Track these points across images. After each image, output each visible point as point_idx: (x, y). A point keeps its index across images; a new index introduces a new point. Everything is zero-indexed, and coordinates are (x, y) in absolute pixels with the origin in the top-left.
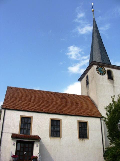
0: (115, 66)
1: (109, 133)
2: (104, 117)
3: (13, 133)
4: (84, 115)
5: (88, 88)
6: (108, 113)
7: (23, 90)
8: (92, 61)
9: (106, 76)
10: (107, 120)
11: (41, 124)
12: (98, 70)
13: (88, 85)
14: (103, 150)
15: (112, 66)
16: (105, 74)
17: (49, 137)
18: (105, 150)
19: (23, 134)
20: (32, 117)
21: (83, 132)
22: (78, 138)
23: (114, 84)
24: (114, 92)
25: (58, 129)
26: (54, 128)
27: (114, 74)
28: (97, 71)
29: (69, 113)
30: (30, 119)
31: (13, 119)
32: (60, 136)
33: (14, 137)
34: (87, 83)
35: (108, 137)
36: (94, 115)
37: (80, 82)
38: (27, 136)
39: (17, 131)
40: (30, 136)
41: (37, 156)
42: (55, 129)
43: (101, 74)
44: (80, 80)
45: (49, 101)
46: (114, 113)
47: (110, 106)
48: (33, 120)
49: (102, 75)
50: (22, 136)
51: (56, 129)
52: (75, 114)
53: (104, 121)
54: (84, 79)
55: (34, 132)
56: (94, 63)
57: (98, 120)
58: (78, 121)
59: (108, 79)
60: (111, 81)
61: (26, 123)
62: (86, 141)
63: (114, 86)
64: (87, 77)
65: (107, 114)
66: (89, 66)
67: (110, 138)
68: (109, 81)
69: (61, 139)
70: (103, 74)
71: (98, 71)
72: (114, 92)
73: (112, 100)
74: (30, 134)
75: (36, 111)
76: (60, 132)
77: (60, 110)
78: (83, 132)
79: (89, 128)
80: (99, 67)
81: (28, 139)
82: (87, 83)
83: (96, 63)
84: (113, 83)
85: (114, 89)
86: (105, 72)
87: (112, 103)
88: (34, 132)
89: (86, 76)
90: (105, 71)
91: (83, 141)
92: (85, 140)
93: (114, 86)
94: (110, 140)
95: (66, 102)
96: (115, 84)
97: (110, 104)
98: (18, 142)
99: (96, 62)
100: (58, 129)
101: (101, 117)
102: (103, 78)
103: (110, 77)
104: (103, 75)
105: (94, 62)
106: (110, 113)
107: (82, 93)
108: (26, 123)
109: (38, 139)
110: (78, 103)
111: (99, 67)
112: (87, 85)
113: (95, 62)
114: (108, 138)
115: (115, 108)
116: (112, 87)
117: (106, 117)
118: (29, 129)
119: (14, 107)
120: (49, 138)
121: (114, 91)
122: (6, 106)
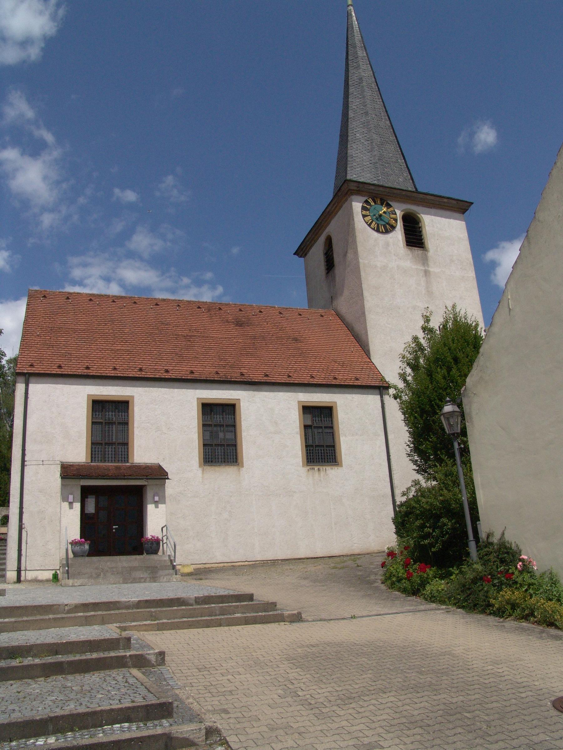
0: (432, 198)
2: (395, 388)
3: (64, 461)
5: (334, 279)
6: (409, 370)
7: (91, 300)
8: (346, 181)
9: (398, 235)
12: (367, 213)
16: (393, 228)
17: (200, 466)
18: (400, 499)
21: (320, 443)
22: (303, 466)
24: (430, 293)
25: (229, 436)
26: (213, 435)
28: (364, 216)
29: (267, 376)
30: (230, 408)
31: (55, 422)
32: (236, 462)
33: (69, 472)
34: (330, 264)
35: (409, 455)
36: (357, 379)
37: (302, 259)
38: (117, 468)
39: (78, 453)
40: (130, 467)
41: (160, 537)
42: (220, 440)
43: (378, 231)
44: (302, 251)
45: (191, 336)
46: (430, 374)
47: (413, 345)
49: (382, 233)
50: (98, 467)
51: (221, 435)
52: (288, 380)
54: (317, 251)
55: (144, 450)
56: (353, 186)
57: (372, 400)
58: (299, 402)
59: (407, 245)
60: (418, 252)
61: (110, 419)
62: (332, 472)
63: (427, 273)
64: (329, 241)
65: (403, 377)
66: (334, 198)
67: (416, 458)
69: (244, 469)
70: (388, 228)
72: (430, 293)
73: (421, 323)
74: (130, 461)
75: (143, 374)
76: (235, 446)
78: (320, 443)
80: (370, 200)
81: (124, 478)
82: (330, 264)
83: (360, 189)
84: (425, 261)
85: (428, 283)
86: (396, 220)
87: (421, 335)
88: (143, 452)
89: (322, 240)
91: (322, 473)
92: (328, 468)
93: (427, 273)
94: (415, 467)
95: (255, 338)
96: (431, 263)
97: (415, 339)
98: (86, 492)
100: (227, 437)
101: (382, 388)
102: (387, 244)
103: (415, 238)
104: (387, 232)
105: (352, 184)
106: (415, 367)
107: (360, 202)
108: (110, 419)
109: (157, 474)
110: (296, 340)
111: (373, 204)
113: (355, 184)
114: (410, 460)
115: (436, 351)
116: (422, 274)
117: (401, 385)
118: (123, 446)
119: (60, 367)
120: (200, 472)
121: (428, 291)
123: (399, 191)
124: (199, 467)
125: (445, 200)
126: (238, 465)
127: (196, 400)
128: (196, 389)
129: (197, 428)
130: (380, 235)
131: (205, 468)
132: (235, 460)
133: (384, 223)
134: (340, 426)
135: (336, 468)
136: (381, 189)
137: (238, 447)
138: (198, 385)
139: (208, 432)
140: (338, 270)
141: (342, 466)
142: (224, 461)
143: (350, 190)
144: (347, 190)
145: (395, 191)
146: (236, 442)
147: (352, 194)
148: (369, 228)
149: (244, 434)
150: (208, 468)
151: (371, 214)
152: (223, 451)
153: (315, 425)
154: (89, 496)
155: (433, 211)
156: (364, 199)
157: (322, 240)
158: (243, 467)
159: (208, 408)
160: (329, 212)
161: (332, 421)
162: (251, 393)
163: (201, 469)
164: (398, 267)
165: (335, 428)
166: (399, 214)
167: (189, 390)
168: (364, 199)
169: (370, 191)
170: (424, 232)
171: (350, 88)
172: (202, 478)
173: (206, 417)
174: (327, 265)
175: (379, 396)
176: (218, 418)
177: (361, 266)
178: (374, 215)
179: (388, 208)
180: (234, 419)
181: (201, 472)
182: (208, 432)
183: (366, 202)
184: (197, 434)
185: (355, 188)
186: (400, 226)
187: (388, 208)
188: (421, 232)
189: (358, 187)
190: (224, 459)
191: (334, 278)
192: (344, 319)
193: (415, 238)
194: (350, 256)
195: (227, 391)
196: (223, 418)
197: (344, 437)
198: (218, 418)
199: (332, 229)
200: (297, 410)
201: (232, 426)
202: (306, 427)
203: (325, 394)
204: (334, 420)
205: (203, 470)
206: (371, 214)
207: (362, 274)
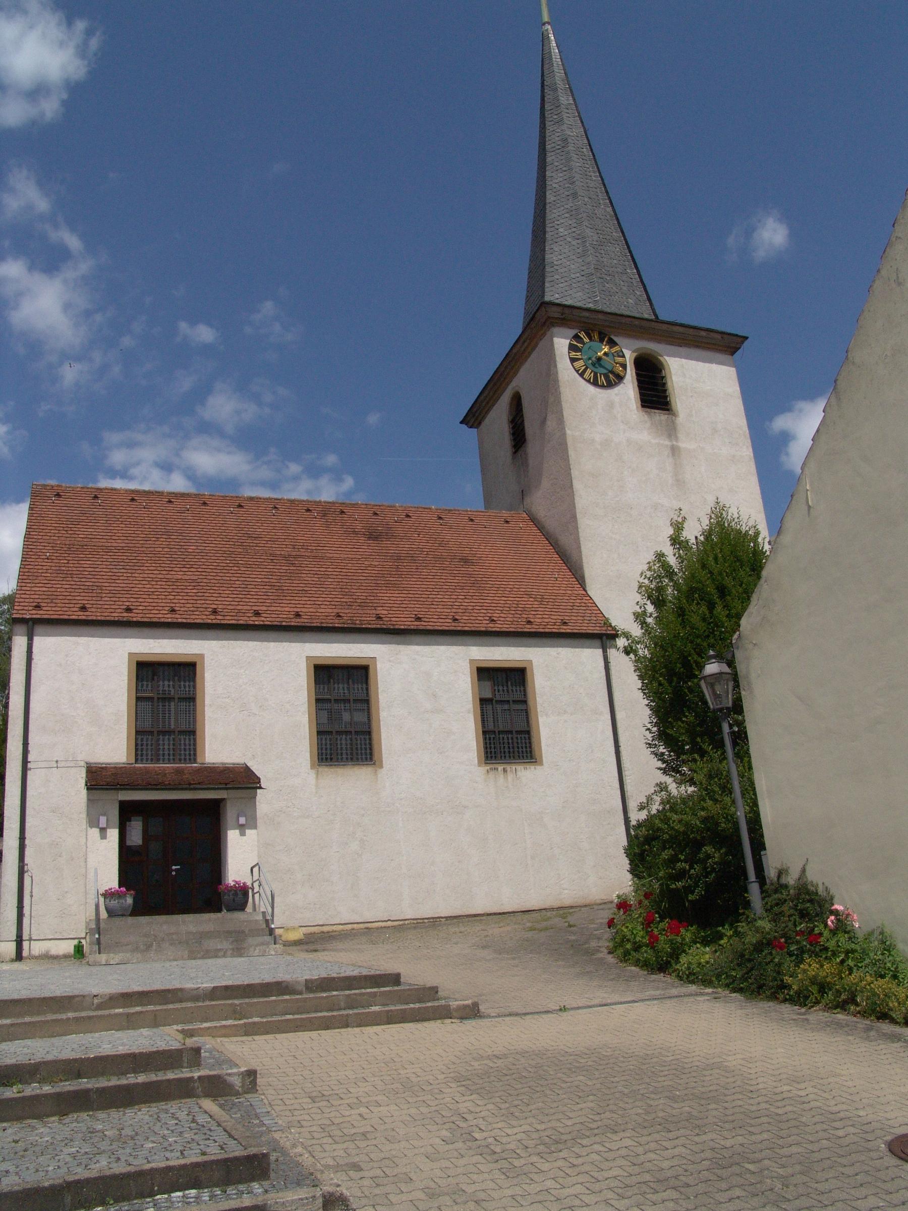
0: (681, 329)
1: (656, 725)
2: (627, 635)
4: (505, 628)
5: (525, 463)
8: (544, 304)
9: (629, 389)
10: (643, 652)
11: (251, 701)
13: (520, 452)
14: (623, 822)
15: (665, 327)
16: (620, 378)
18: (637, 816)
19: (158, 760)
20: (202, 656)
21: (507, 727)
22: (480, 764)
23: (677, 439)
24: (679, 482)
25: (359, 717)
26: (333, 717)
27: (674, 378)
28: (573, 360)
29: (418, 619)
30: (186, 671)
31: (80, 694)
32: (371, 759)
33: (99, 779)
36: (565, 623)
38: (179, 771)
39: (116, 749)
41: (249, 884)
42: (344, 724)
43: (595, 383)
45: (296, 557)
46: (681, 613)
48: (208, 676)
50: (147, 771)
51: (346, 716)
53: (627, 651)
54: (498, 417)
55: (221, 743)
56: (554, 312)
57: (589, 657)
58: (472, 661)
59: (643, 406)
60: (660, 416)
61: (167, 693)
62: (525, 774)
63: (674, 451)
64: (517, 402)
65: (640, 617)
69: (382, 773)
70: (612, 380)
71: (581, 363)
72: (679, 482)
74: (199, 760)
77: (363, 605)
78: (507, 727)
79: (539, 700)
80: (582, 335)
82: (519, 438)
83: (566, 316)
84: (671, 431)
86: (624, 366)
88: (219, 746)
89: (505, 399)
90: (620, 360)
91: (510, 776)
92: (520, 768)
93: (674, 451)
94: (660, 764)
95: (399, 558)
96: (681, 436)
98: (127, 811)
99: (722, 333)
100: (355, 719)
101: (605, 637)
102: (611, 405)
103: (655, 394)
104: (610, 385)
105: (555, 309)
106: (659, 602)
108: (167, 693)
109: (244, 781)
110: (465, 561)
111: (586, 340)
112: (514, 446)
114: (653, 753)
117: (636, 631)
118: (189, 736)
119: (83, 608)
120: (312, 775)
121: (678, 480)
122: (38, 607)
125: (703, 333)
126: (374, 764)
129: (306, 705)
130: (598, 390)
131: (320, 769)
135: (533, 767)
136: (600, 316)
137: (374, 736)
138: (308, 635)
140: (532, 447)
142: (352, 759)
147: (553, 325)
148: (580, 379)
151: (585, 357)
153: (498, 698)
156: (573, 332)
157: (505, 399)
158: (381, 767)
160: (516, 354)
162: (393, 647)
166: (629, 356)
168: (573, 332)
170: (669, 384)
171: (548, 154)
172: (317, 786)
173: (322, 686)
178: (590, 359)
180: (367, 689)
183: (576, 337)
187: (611, 348)
190: (352, 754)
192: (543, 527)
193: (655, 394)
194: (551, 424)
195: (355, 645)
196: (348, 689)
199: (522, 381)
202: (483, 702)
204: (529, 690)
205: (317, 774)
207: (571, 453)
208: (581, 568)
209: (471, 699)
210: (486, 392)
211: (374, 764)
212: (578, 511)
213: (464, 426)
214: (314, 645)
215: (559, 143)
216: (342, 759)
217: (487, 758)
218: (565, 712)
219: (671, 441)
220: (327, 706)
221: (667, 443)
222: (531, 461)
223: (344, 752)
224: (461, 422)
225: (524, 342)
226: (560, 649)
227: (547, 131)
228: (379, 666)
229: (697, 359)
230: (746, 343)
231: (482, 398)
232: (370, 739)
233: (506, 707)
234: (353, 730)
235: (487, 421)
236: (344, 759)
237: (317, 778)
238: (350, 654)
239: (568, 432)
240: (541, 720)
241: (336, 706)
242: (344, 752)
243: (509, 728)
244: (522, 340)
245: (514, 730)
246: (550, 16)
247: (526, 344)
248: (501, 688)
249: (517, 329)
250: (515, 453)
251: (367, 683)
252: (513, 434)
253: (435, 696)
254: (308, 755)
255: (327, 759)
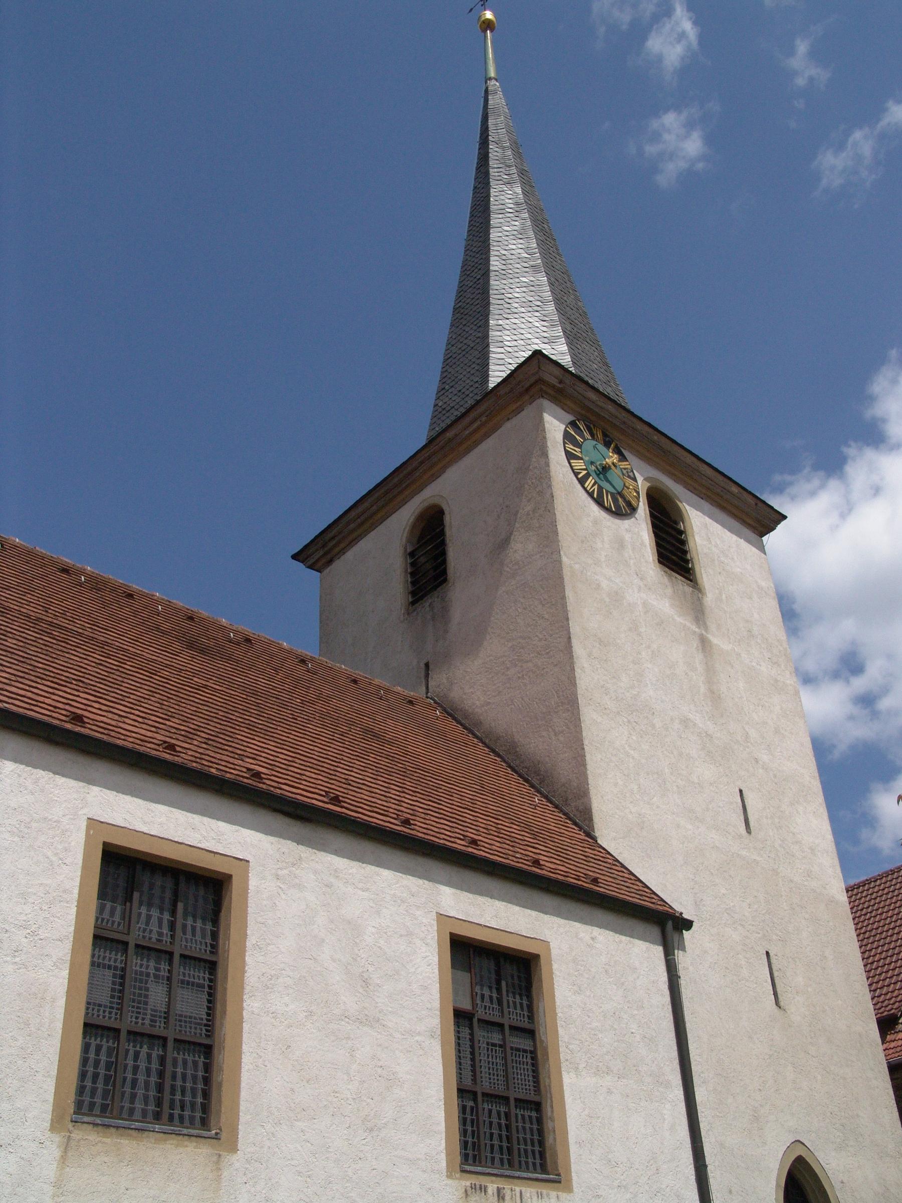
0: (709, 472)
9: (639, 530)
17: (56, 1124)
25: (190, 1004)
28: (570, 456)
30: (206, 890)
32: (205, 1123)
43: (599, 502)
49: (608, 510)
51: (157, 995)
63: (704, 643)
68: (666, 580)
69: (236, 1162)
70: (622, 509)
71: (578, 465)
85: (710, 672)
89: (401, 521)
93: (704, 643)
104: (618, 513)
112: (413, 593)
113: (557, 371)
116: (695, 643)
120: (52, 1149)
123: (647, 428)
124: (53, 1129)
125: (735, 489)
126: (217, 1137)
127: (84, 825)
128: (91, 782)
129: (68, 945)
130: (603, 514)
131: (77, 1135)
132: (198, 1115)
133: (614, 491)
134: (561, 1031)
135: (553, 1194)
136: (610, 407)
137: (224, 1059)
138: (101, 768)
139: (109, 973)
140: (462, 593)
141: (569, 1189)
142: (157, 1117)
143: (540, 381)
144: (532, 380)
145: (639, 426)
146: (210, 1033)
147: (543, 394)
148: (579, 486)
149: (252, 1005)
150: (90, 1138)
151: (587, 459)
152: (155, 1066)
153: (480, 1013)
154: (851, 451)
155: (706, 505)
156: (571, 418)
157: (401, 521)
158: (233, 1148)
159: (123, 869)
160: (450, 440)
161: (530, 1008)
162: (288, 847)
163: (57, 1138)
164: (645, 604)
165: (541, 1034)
166: (642, 485)
167: (61, 780)
168: (571, 418)
169: (587, 403)
170: (691, 544)
171: (493, 216)
172: (58, 1184)
173: (109, 905)
174: (413, 583)
175: (661, 949)
176: (154, 921)
177: (566, 573)
178: (592, 463)
179: (619, 461)
180: (215, 936)
181: (57, 1153)
182: (109, 973)
183: (573, 424)
184: (65, 973)
185: (554, 381)
186: (643, 509)
187: (619, 461)
188: (683, 542)
189: (560, 382)
190: (159, 1103)
191: (443, 615)
192: (478, 724)
193: (674, 553)
194: (522, 546)
195: (206, 820)
196: (172, 926)
197: (572, 1075)
198: (154, 921)
199: (450, 488)
200: (435, 945)
201: (208, 968)
202: (461, 1017)
203: (517, 909)
204: (542, 1007)
205: (66, 1148)
206: (587, 459)
207: (569, 593)
208: (583, 793)
209: (437, 1004)
210: (366, 505)
211: (217, 1137)
212: (580, 692)
213: (299, 566)
214: (110, 796)
215: (512, 206)
216: (132, 1111)
217: (465, 1158)
218: (609, 1071)
219: (699, 628)
220: (115, 958)
221: (694, 628)
222: (456, 614)
223: (140, 1092)
224: (295, 557)
225: (475, 420)
226: (596, 931)
227: (492, 190)
228: (253, 883)
229: (723, 525)
230: (783, 523)
231: (353, 514)
232: (208, 1068)
233: (496, 1038)
234: (171, 1035)
235: (339, 565)
236: (137, 1115)
237: (64, 1158)
238: (193, 838)
239: (564, 559)
240: (568, 1079)
241: (136, 963)
242: (140, 1092)
243: (500, 1090)
244: (472, 415)
245: (512, 1096)
246: (497, 70)
247: (477, 424)
248: (486, 992)
249: (416, 437)
250: (413, 603)
251: (215, 921)
252: (412, 574)
253: (366, 982)
254: (50, 1086)
255: (92, 1105)
